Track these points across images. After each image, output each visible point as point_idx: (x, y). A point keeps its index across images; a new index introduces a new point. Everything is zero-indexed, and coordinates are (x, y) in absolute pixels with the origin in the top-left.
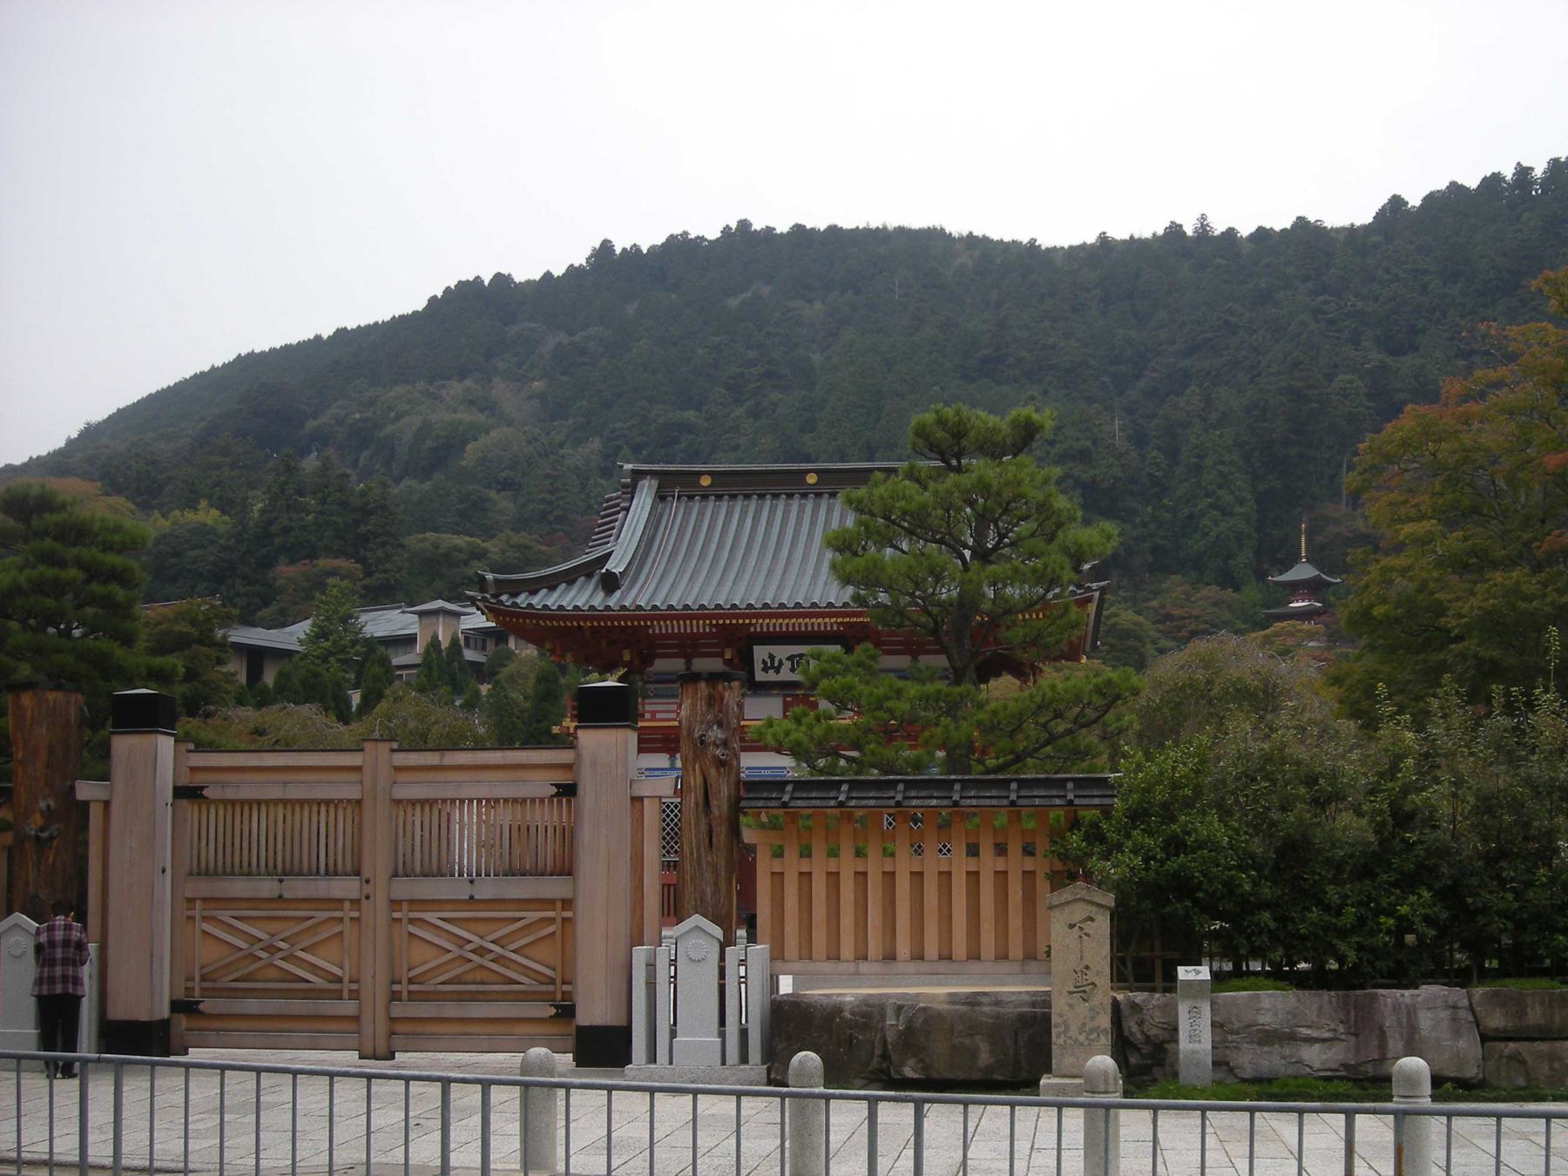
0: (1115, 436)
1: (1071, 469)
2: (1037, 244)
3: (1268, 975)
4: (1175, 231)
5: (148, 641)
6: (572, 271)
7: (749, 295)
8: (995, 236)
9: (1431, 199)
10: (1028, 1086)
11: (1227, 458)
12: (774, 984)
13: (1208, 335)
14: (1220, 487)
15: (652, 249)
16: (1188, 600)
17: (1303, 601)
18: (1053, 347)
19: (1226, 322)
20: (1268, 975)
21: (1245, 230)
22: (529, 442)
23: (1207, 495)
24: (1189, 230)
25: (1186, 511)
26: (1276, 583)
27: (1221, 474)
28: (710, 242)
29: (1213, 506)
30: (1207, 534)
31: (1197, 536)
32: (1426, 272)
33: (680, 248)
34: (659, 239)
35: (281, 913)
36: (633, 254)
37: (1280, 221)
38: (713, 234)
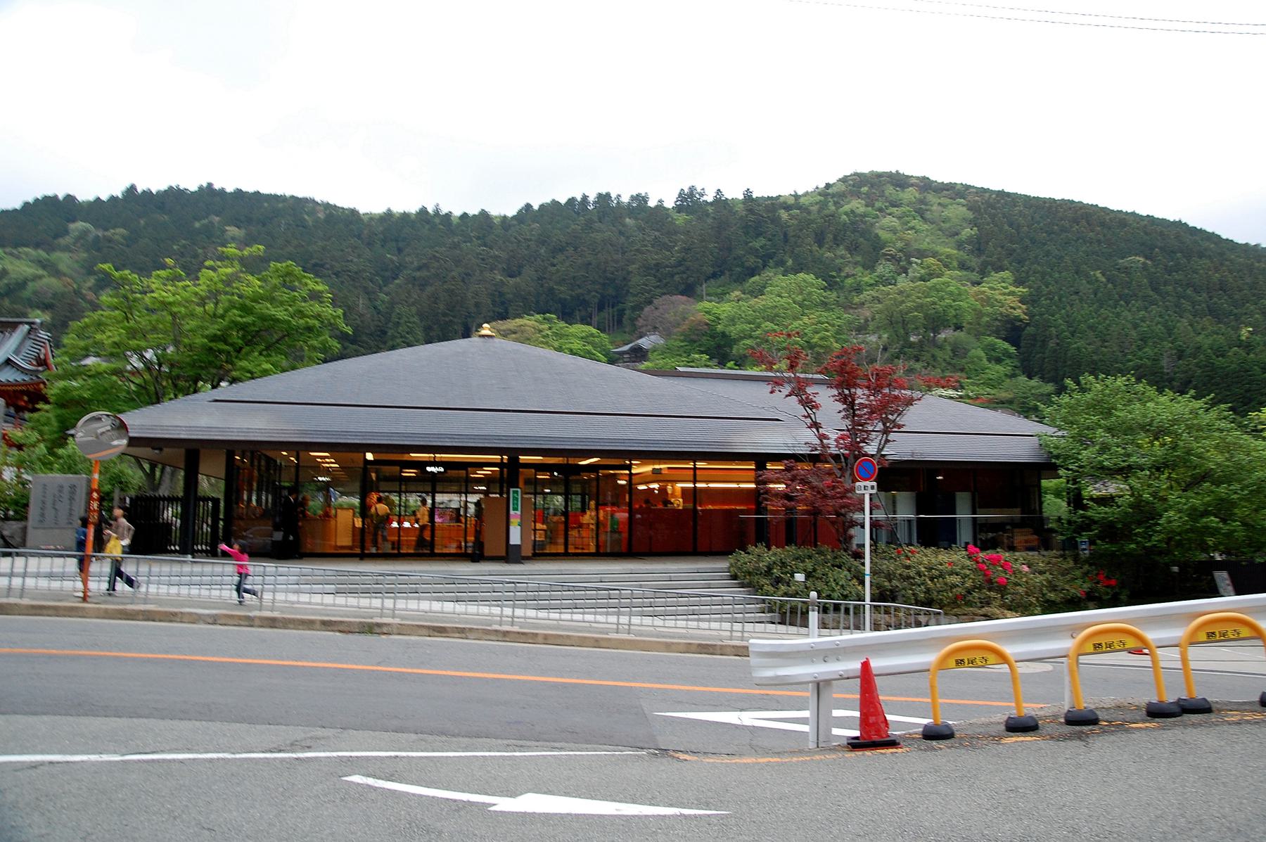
2: (652, 203)
3: (206, 552)
4: (423, 211)
5: (15, 494)
6: (113, 199)
8: (339, 204)
9: (542, 206)
10: (1032, 731)
11: (411, 320)
12: (1061, 723)
15: (158, 192)
19: (434, 256)
20: (206, 552)
21: (457, 213)
24: (430, 210)
28: (192, 192)
32: (531, 240)
33: (174, 195)
34: (164, 187)
36: (147, 194)
37: (473, 211)
38: (193, 187)
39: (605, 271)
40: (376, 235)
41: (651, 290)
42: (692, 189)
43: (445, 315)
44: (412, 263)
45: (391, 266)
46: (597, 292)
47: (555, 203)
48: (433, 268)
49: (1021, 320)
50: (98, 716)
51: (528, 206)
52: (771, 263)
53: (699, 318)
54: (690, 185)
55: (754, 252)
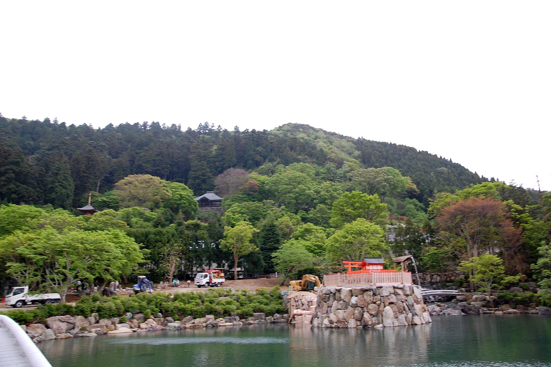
13: (57, 145)
25: (51, 186)
26: (80, 210)
27: (64, 176)
30: (57, 193)
39: (173, 158)
40: (18, 129)
41: (205, 169)
42: (206, 124)
43: (84, 172)
44: (44, 146)
45: (29, 147)
46: (169, 169)
47: (128, 125)
48: (63, 149)
49: (415, 192)
50: (416, 296)
51: (111, 125)
52: (267, 160)
53: (19, 252)
54: (205, 122)
55: (259, 153)
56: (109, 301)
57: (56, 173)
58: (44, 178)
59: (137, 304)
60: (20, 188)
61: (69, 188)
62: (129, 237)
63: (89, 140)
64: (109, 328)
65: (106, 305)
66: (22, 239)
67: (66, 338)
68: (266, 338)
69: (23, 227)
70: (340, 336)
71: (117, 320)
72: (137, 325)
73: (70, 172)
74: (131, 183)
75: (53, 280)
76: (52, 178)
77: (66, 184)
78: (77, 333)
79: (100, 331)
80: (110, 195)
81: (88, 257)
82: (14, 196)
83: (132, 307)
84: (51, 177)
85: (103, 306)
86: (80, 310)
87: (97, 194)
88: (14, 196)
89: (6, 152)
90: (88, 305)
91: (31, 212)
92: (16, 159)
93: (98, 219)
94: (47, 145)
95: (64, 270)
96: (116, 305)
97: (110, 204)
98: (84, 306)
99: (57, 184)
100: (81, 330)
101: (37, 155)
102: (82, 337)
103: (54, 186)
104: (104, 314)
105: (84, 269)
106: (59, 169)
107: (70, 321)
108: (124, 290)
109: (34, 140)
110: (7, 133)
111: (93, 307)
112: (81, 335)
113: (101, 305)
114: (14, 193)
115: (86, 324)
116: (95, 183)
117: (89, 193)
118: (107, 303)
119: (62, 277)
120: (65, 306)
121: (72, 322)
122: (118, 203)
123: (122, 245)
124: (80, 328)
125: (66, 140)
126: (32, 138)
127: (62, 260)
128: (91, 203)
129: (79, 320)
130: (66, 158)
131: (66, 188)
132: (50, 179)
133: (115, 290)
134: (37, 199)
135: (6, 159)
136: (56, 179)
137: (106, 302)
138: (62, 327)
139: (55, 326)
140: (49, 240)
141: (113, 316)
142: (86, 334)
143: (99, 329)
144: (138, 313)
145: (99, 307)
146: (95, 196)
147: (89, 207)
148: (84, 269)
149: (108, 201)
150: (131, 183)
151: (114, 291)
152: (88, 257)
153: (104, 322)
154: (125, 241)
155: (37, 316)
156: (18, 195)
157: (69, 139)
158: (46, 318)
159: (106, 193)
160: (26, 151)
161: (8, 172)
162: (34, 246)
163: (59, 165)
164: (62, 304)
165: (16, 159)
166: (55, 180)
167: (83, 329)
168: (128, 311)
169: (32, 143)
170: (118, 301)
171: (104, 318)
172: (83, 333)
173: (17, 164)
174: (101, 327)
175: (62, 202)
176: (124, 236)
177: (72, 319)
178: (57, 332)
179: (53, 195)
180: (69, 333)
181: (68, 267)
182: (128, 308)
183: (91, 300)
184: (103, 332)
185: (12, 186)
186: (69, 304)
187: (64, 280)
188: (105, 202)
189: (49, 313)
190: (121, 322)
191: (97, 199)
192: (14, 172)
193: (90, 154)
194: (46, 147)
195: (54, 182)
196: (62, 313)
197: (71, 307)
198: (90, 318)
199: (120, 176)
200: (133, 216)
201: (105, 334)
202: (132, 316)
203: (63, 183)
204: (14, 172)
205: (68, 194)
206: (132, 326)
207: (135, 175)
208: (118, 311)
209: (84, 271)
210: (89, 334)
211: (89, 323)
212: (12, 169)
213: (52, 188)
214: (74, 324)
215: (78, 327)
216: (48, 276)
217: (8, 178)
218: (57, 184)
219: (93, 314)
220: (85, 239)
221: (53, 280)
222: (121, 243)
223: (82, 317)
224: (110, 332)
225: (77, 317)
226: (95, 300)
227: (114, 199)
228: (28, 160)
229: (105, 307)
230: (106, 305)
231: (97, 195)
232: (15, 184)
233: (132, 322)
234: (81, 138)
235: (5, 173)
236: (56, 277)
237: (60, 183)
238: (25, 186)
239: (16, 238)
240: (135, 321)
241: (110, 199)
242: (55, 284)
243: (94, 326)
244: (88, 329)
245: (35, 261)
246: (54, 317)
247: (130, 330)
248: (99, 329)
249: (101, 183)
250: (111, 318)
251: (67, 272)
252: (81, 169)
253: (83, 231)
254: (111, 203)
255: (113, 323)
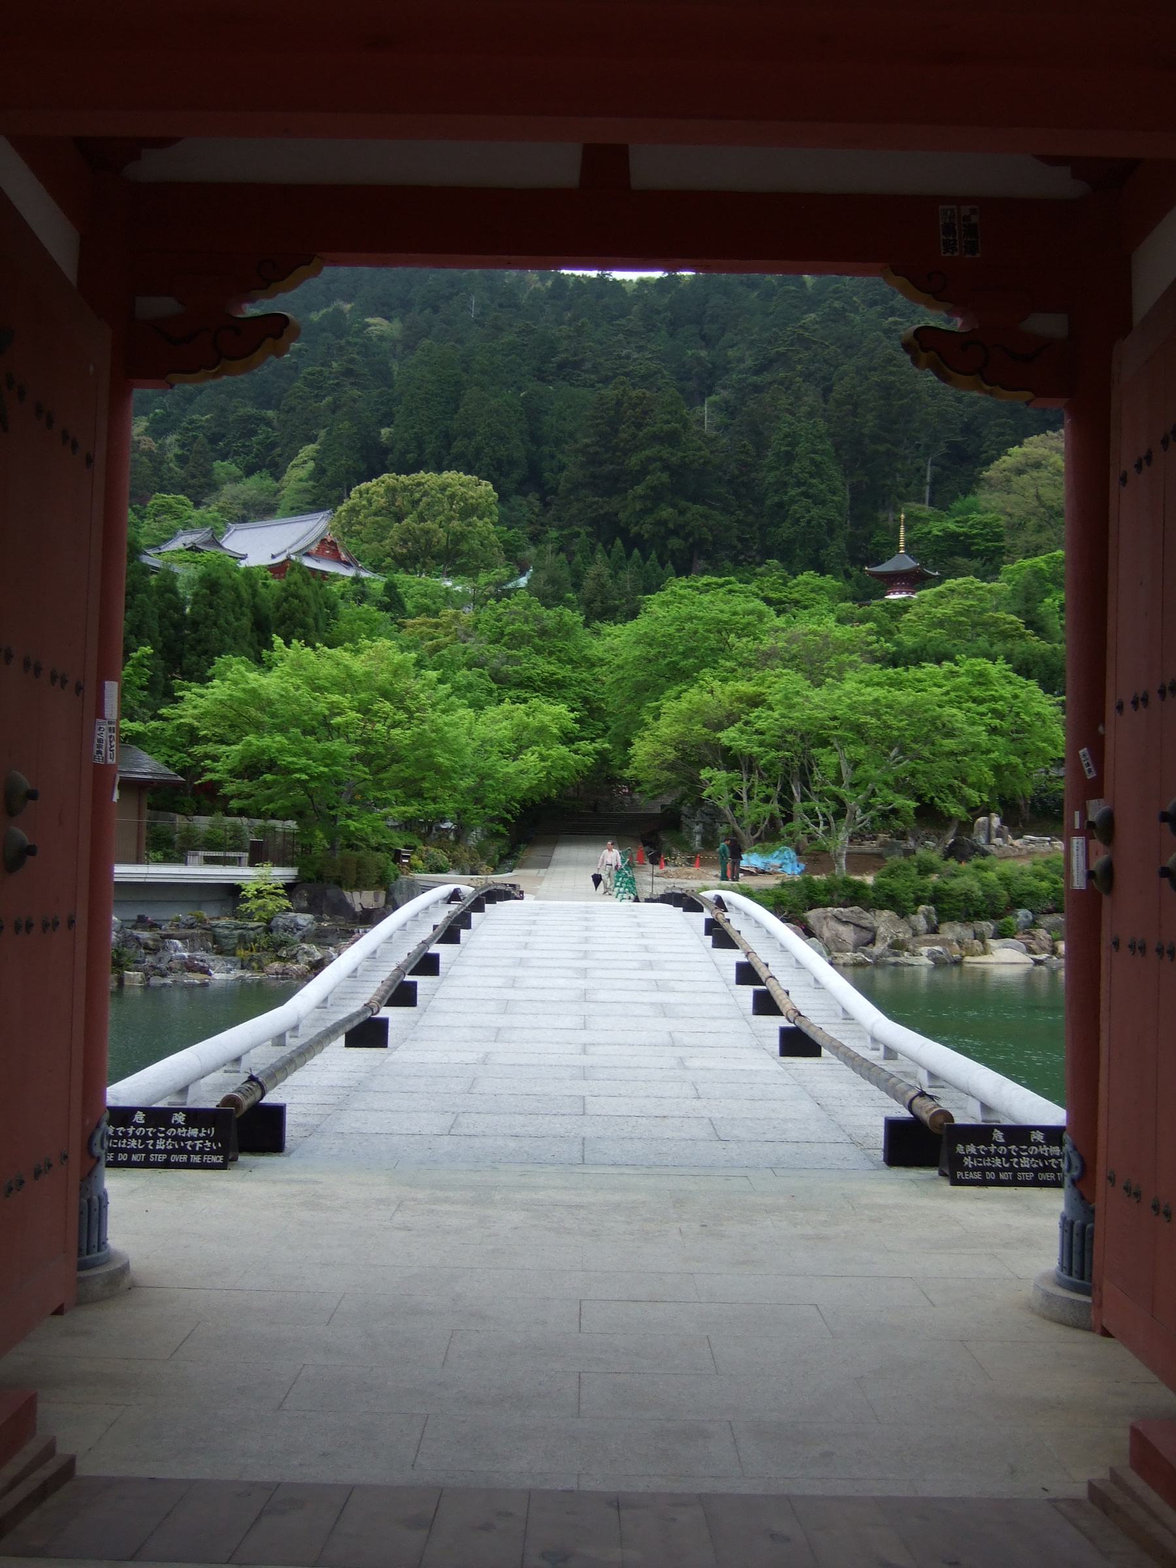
0: (703, 423)
1: (659, 452)
7: (330, 309)
13: (782, 349)
14: (812, 476)
16: (785, 584)
17: (901, 592)
18: (628, 357)
22: (433, 731)
23: (799, 484)
25: (776, 499)
26: (873, 574)
27: (813, 461)
29: (806, 495)
30: (798, 521)
31: (787, 524)
35: (150, 777)
40: (658, 312)
44: (741, 360)
48: (800, 361)
56: (964, 873)
57: (787, 453)
58: (753, 475)
59: (1045, 884)
60: (689, 515)
61: (833, 501)
62: (1021, 679)
63: (884, 315)
64: (966, 949)
65: (954, 884)
66: (721, 697)
67: (854, 965)
68: (545, 864)
69: (722, 662)
70: (211, 833)
71: (987, 926)
72: (1046, 944)
73: (828, 445)
74: (1037, 465)
75: (811, 814)
76: (778, 473)
77: (823, 487)
78: (882, 955)
79: (941, 953)
80: (970, 510)
81: (895, 750)
82: (675, 543)
83: (1030, 894)
84: (772, 469)
85: (947, 887)
86: (887, 896)
87: (925, 510)
88: (675, 543)
89: (636, 405)
90: (909, 884)
91: (735, 613)
92: (668, 422)
93: (929, 613)
94: (750, 356)
95: (834, 788)
96: (984, 885)
97: (973, 544)
98: (896, 884)
99: (793, 492)
100: (891, 946)
101: (725, 393)
102: (896, 964)
103: (785, 498)
104: (951, 909)
105: (886, 783)
106: (792, 439)
107: (864, 923)
108: (1017, 843)
109: (707, 341)
110: (630, 333)
111: (920, 890)
112: (892, 959)
113: (942, 885)
114: (674, 533)
115: (904, 934)
116: (918, 470)
117: (899, 511)
118: (959, 880)
119: (833, 805)
120: (847, 884)
121: (868, 925)
122: (998, 537)
123: (999, 706)
124: (889, 941)
125: (806, 329)
126: (703, 337)
127: (827, 758)
128: (909, 544)
129: (884, 921)
130: (811, 397)
131: (823, 503)
132: (771, 477)
133: (989, 842)
134: (740, 546)
135: (639, 426)
136: (789, 473)
137: (955, 876)
138: (844, 936)
139: (827, 934)
140: (791, 707)
141: (978, 916)
142: (906, 958)
143: (937, 948)
144: (1050, 912)
145: (936, 890)
146: (918, 519)
147: (902, 562)
148: (886, 783)
149: (965, 534)
150: (1037, 465)
151: (986, 847)
152: (895, 750)
153: (952, 931)
154: (1007, 691)
155: (782, 903)
156: (685, 539)
157: (817, 323)
158: (804, 910)
159: (957, 505)
160: (692, 385)
161: (651, 468)
162: (757, 726)
163: (793, 424)
164: (840, 878)
165: (668, 422)
166: (787, 479)
167: (897, 946)
168: (1020, 905)
169: (703, 353)
170: (991, 876)
171: (952, 919)
172: (896, 955)
173: (671, 438)
174: (945, 943)
175: (817, 551)
176: (1006, 677)
177: (868, 918)
178: (833, 947)
179: (786, 531)
180: (863, 952)
181: (847, 779)
182: (1021, 895)
183: (915, 871)
184: (948, 957)
185: (666, 512)
186: (857, 878)
187: (840, 814)
188: (954, 536)
189: (809, 898)
190: (1000, 934)
191: (926, 530)
192: (666, 467)
193: (891, 373)
194: (749, 362)
195: (785, 484)
196: (842, 900)
197: (862, 886)
198: (913, 917)
199: (1002, 434)
200: (1050, 586)
201: (958, 963)
202: (1031, 918)
203: (811, 486)
204: (666, 467)
205: (830, 522)
206: (1034, 946)
207: (1050, 433)
208: (993, 904)
209: (886, 791)
210: (912, 960)
211: (911, 931)
212: (661, 459)
213: (780, 505)
214: (873, 931)
215: (884, 939)
216: (798, 806)
217: (653, 488)
218: (793, 492)
219: (922, 908)
220: (884, 701)
221: (811, 814)
222: (994, 699)
223: (892, 913)
224: (968, 959)
225: (878, 912)
226: (926, 869)
227: (985, 525)
228: (700, 422)
229: (952, 889)
230: (956, 886)
231: (924, 514)
232: (674, 506)
233: (1034, 937)
234: (856, 311)
235: (644, 471)
236: (817, 806)
237: (803, 488)
238: (699, 508)
239: (707, 697)
240: (1041, 933)
241: (972, 527)
242: (817, 824)
243: (925, 940)
244: (911, 947)
245: (764, 765)
246: (821, 910)
247: (1027, 959)
248: (937, 948)
249: (939, 469)
250: (972, 922)
251: (843, 791)
252: (866, 431)
253: (881, 669)
254: (976, 541)
255: (980, 936)
